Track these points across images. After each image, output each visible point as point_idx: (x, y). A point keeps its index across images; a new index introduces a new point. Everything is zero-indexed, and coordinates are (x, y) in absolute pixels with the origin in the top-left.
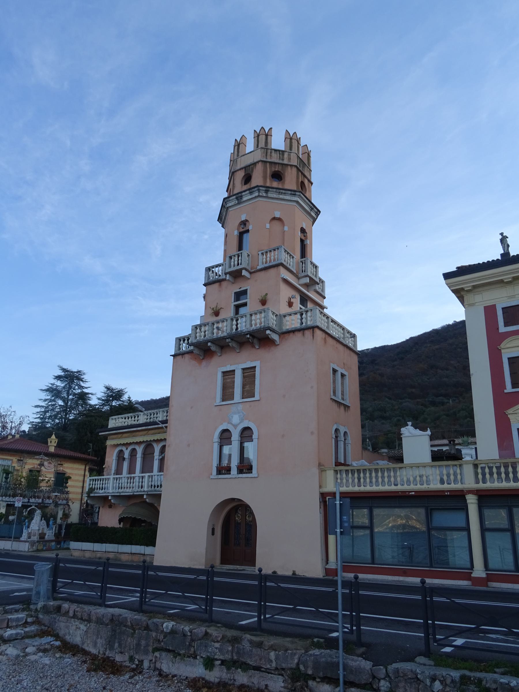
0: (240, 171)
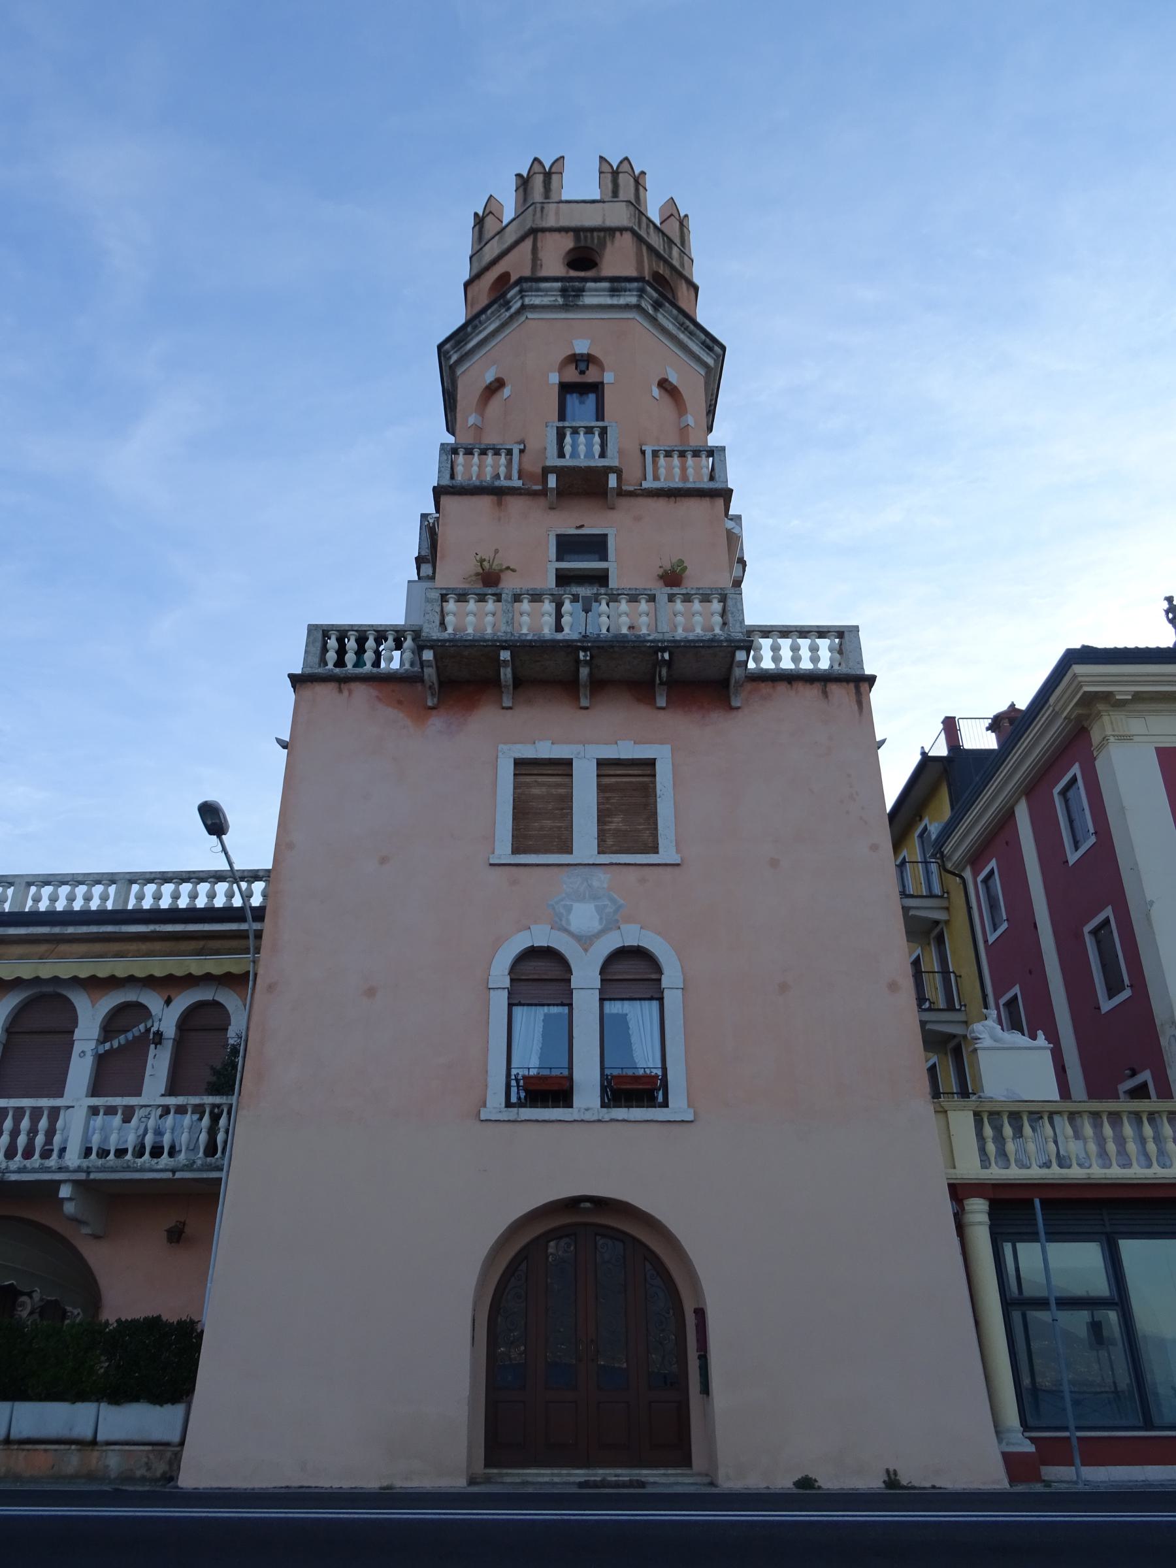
0: (556, 236)
